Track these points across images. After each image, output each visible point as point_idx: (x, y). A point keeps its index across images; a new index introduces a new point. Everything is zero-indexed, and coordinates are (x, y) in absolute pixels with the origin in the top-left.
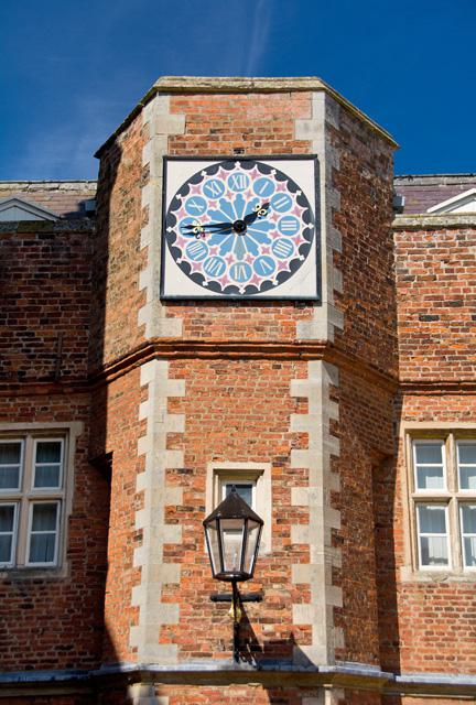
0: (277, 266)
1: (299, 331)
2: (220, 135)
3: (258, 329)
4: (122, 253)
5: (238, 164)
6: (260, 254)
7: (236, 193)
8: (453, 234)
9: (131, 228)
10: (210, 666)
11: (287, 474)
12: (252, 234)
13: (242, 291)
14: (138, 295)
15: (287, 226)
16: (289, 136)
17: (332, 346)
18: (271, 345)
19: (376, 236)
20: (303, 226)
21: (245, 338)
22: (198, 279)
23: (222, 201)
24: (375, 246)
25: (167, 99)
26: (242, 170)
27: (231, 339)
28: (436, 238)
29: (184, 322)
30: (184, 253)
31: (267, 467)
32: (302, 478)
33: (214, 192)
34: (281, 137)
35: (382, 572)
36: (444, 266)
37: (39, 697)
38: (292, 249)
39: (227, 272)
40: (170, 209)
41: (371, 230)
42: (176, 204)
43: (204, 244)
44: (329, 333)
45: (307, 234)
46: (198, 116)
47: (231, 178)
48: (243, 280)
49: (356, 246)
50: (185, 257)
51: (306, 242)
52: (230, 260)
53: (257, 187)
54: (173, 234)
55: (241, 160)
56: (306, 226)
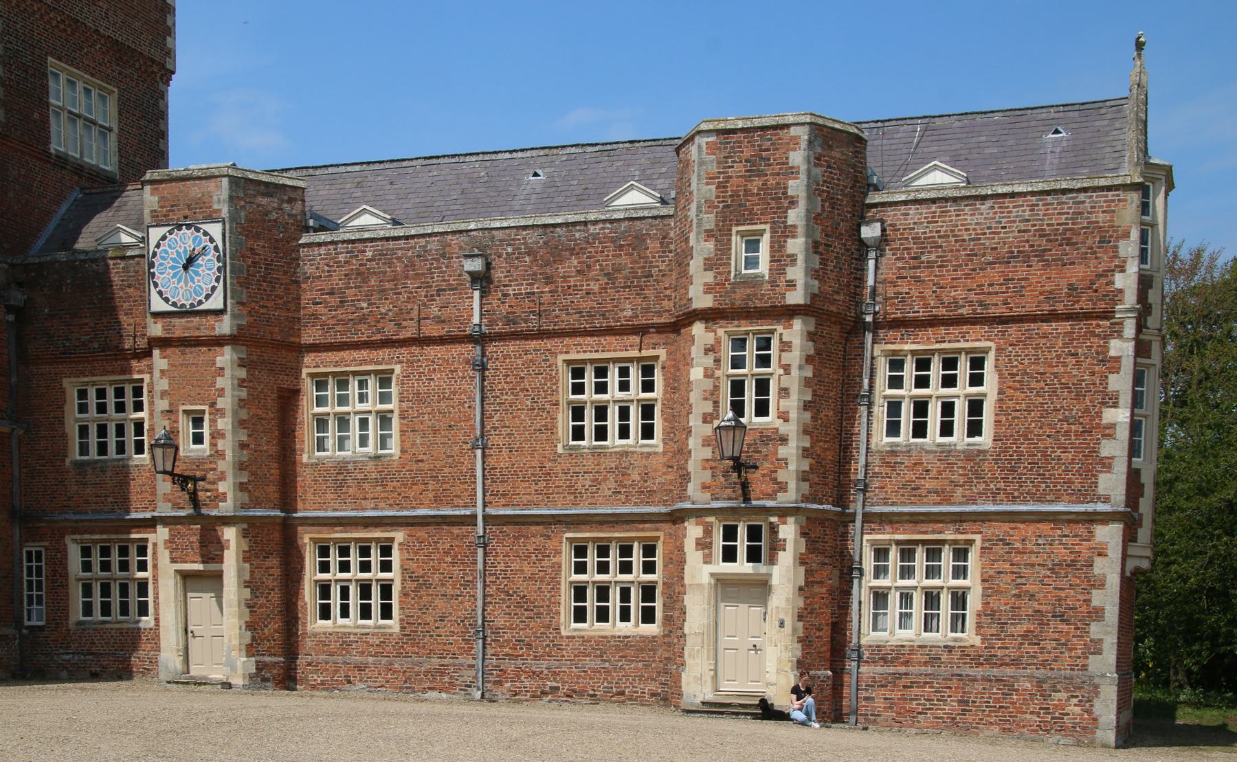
8: (332, 247)
10: (182, 513)
11: (217, 412)
15: (210, 265)
28: (323, 250)
31: (206, 408)
32: (222, 413)
36: (326, 268)
37: (484, 484)
45: (219, 269)
53: (194, 240)
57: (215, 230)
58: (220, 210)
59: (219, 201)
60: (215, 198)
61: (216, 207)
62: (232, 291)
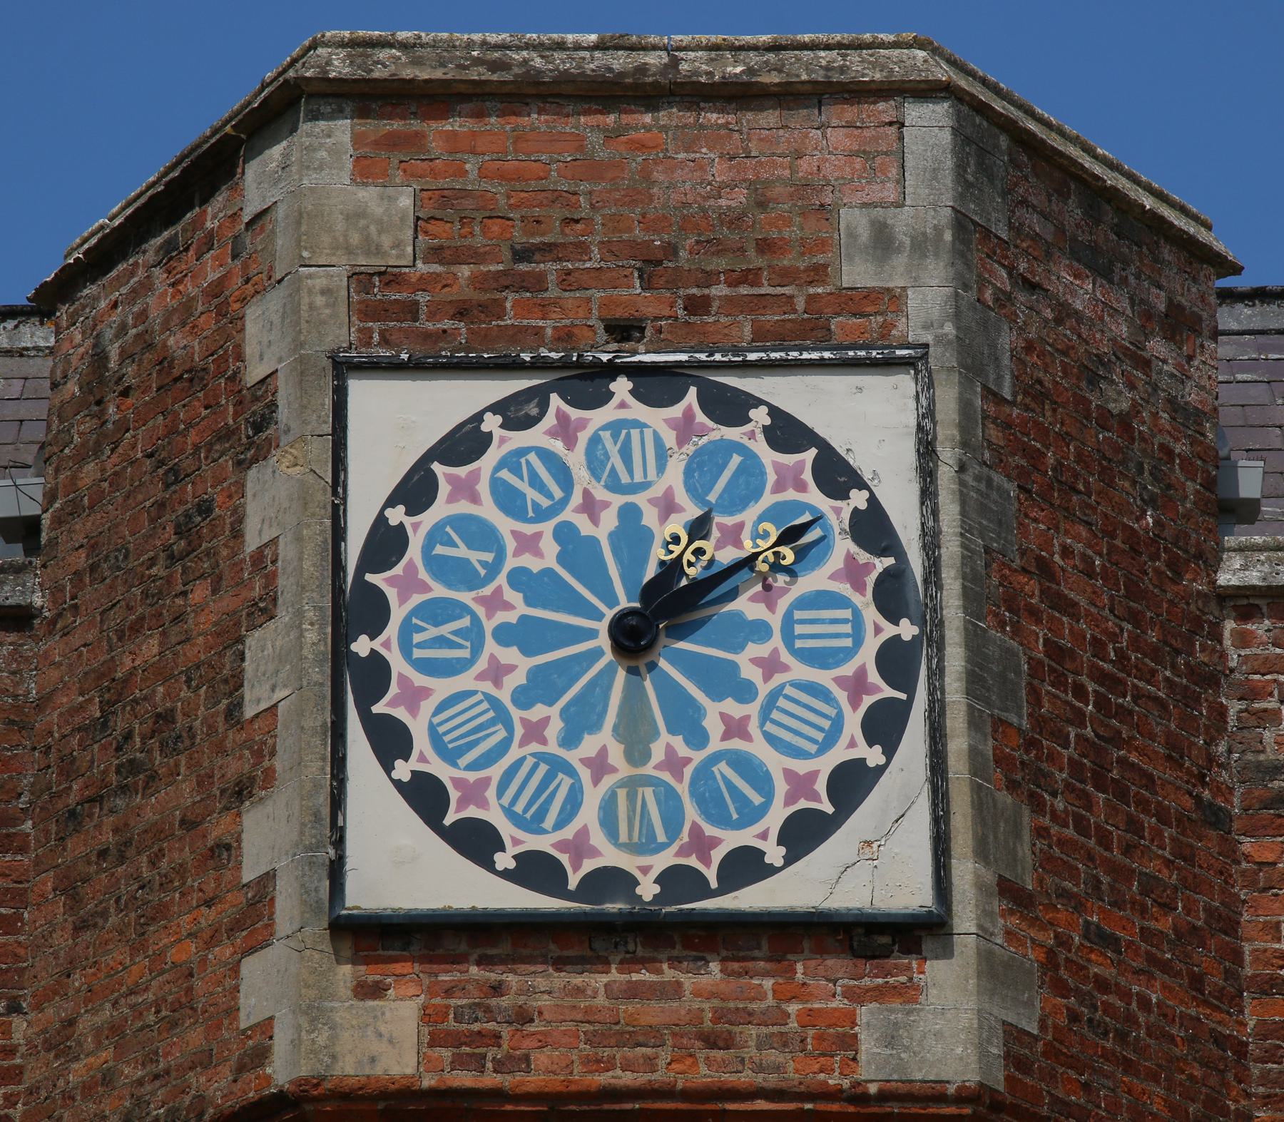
0: (781, 787)
1: (868, 1045)
2: (551, 269)
3: (711, 1041)
4: (166, 717)
5: (621, 386)
6: (715, 745)
7: (618, 500)
9: (202, 623)
12: (682, 661)
13: (648, 890)
14: (241, 898)
15: (824, 629)
16: (818, 273)
17: (997, 1105)
18: (761, 1105)
19: (1153, 636)
20: (879, 630)
21: (660, 1076)
22: (476, 842)
23: (565, 534)
24: (1150, 677)
25: (341, 131)
26: (639, 411)
27: (603, 1079)
29: (428, 1016)
30: (421, 741)
33: (532, 494)
34: (787, 276)
35: (1078, 387)
38: (838, 723)
39: (588, 815)
40: (360, 571)
41: (1135, 618)
42: (385, 545)
43: (494, 703)
44: (983, 1054)
45: (895, 660)
46: (464, 193)
47: (595, 440)
48: (648, 846)
49: (1080, 691)
50: (424, 758)
51: (889, 692)
52: (599, 766)
53: (701, 469)
54: (378, 665)
55: (635, 371)
56: (890, 630)
57: (870, 419)
58: (893, 300)
59: (883, 242)
60: (854, 220)
61: (857, 273)
62: (981, 804)
